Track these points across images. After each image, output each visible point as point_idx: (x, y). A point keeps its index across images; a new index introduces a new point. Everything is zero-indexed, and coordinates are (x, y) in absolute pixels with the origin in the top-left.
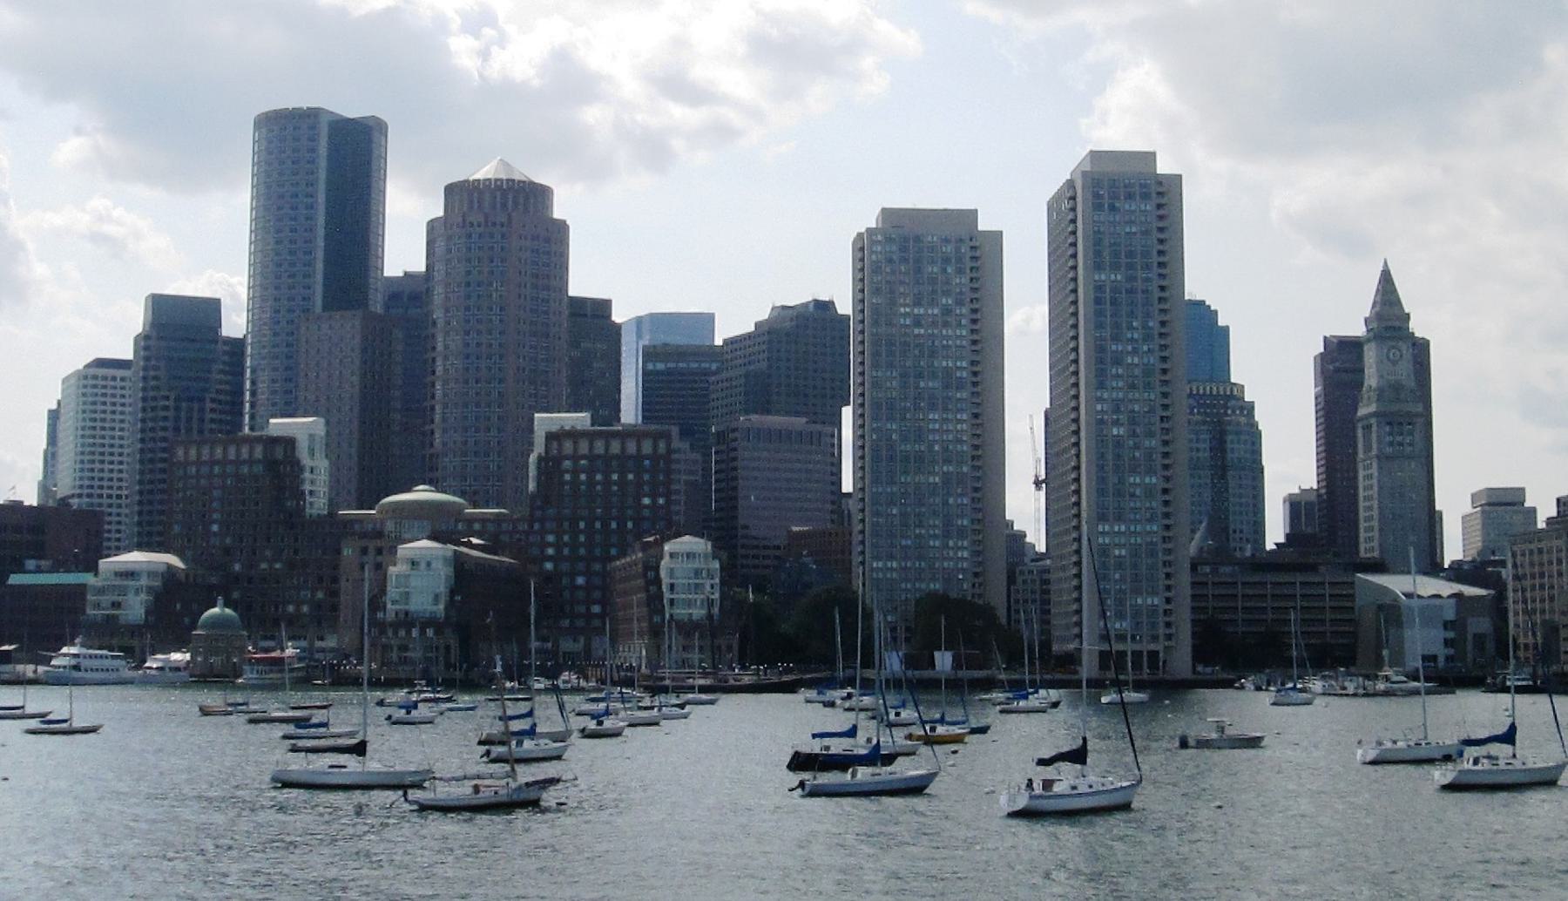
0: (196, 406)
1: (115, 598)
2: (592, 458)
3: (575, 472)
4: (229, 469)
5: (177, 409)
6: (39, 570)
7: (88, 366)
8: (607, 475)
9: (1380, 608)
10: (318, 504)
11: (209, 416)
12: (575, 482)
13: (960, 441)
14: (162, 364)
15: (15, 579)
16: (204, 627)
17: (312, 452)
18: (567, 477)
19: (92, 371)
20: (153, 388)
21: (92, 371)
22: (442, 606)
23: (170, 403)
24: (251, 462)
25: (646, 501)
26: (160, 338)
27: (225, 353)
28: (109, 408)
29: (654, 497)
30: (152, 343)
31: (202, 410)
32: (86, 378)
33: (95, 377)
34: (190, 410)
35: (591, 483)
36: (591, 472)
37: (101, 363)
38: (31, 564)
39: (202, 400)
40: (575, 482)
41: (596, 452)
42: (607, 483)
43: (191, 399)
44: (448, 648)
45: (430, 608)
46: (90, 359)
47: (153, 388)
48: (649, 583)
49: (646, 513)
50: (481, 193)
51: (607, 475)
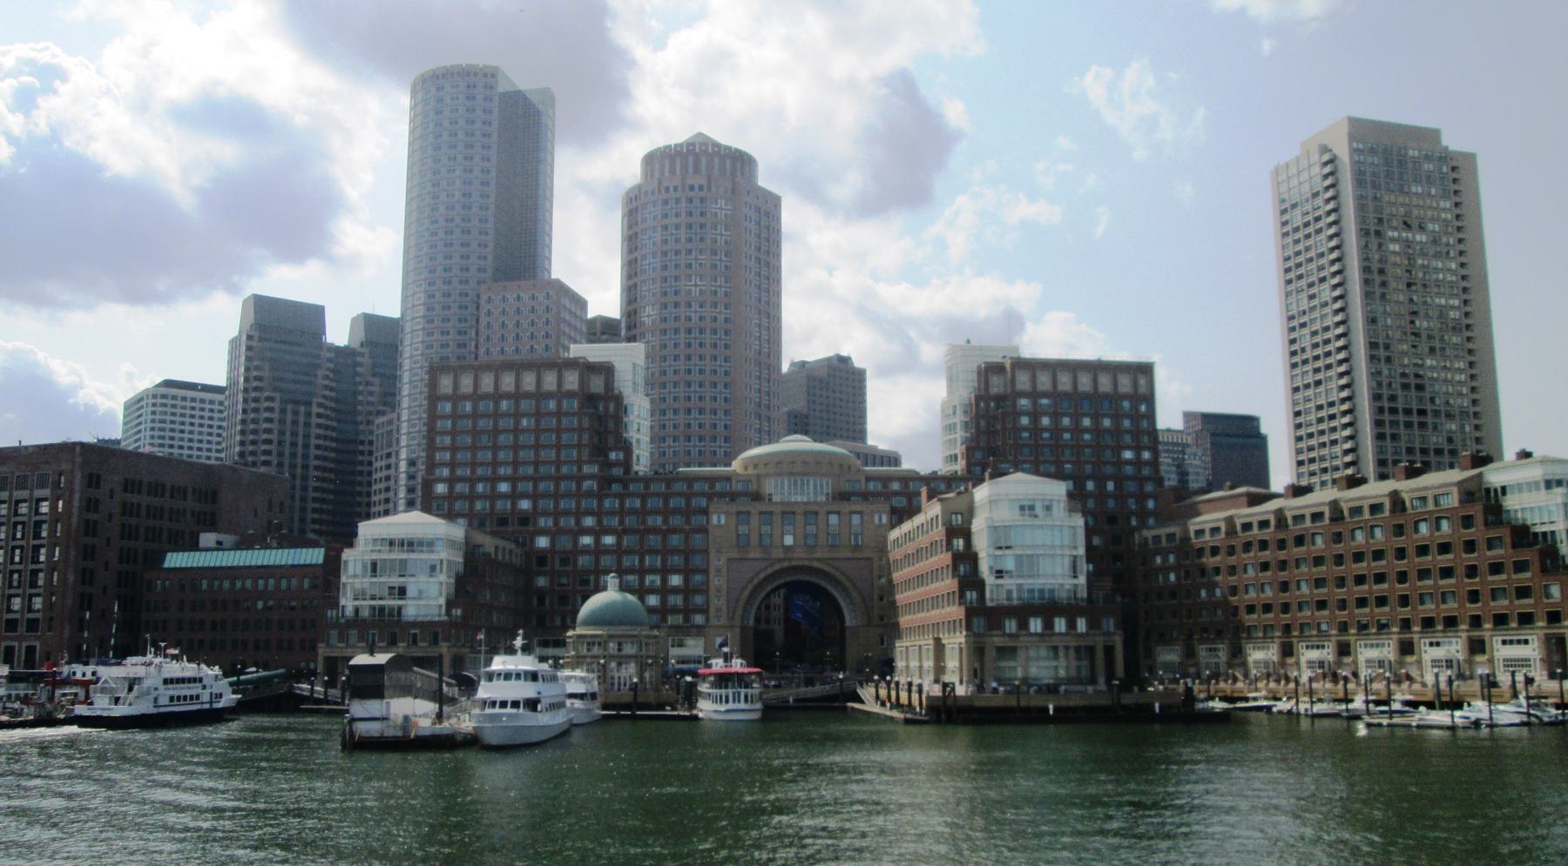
0: (302, 409)
1: (396, 581)
2: (1055, 395)
3: (1035, 415)
4: (525, 405)
5: (283, 411)
6: (220, 546)
7: (158, 386)
8: (1076, 418)
9: (794, 588)
10: (643, 461)
11: (315, 420)
12: (1036, 429)
13: (1460, 394)
14: (267, 366)
15: (175, 560)
16: (593, 621)
17: (635, 390)
18: (1025, 421)
19: (164, 390)
20: (256, 389)
21: (164, 390)
22: (1082, 580)
23: (276, 405)
24: (560, 395)
25: (1128, 455)
26: (261, 340)
27: (330, 360)
28: (188, 420)
29: (1138, 449)
30: (254, 344)
31: (309, 414)
32: (155, 396)
33: (164, 396)
34: (296, 413)
35: (1056, 431)
36: (1056, 416)
37: (168, 384)
38: (207, 539)
39: (309, 404)
40: (1036, 429)
41: (1061, 388)
42: (1077, 430)
43: (296, 402)
44: (1109, 650)
45: (1069, 582)
46: (159, 380)
47: (256, 389)
48: (958, 558)
49: (1129, 470)
50: (697, 157)
51: (1076, 418)
